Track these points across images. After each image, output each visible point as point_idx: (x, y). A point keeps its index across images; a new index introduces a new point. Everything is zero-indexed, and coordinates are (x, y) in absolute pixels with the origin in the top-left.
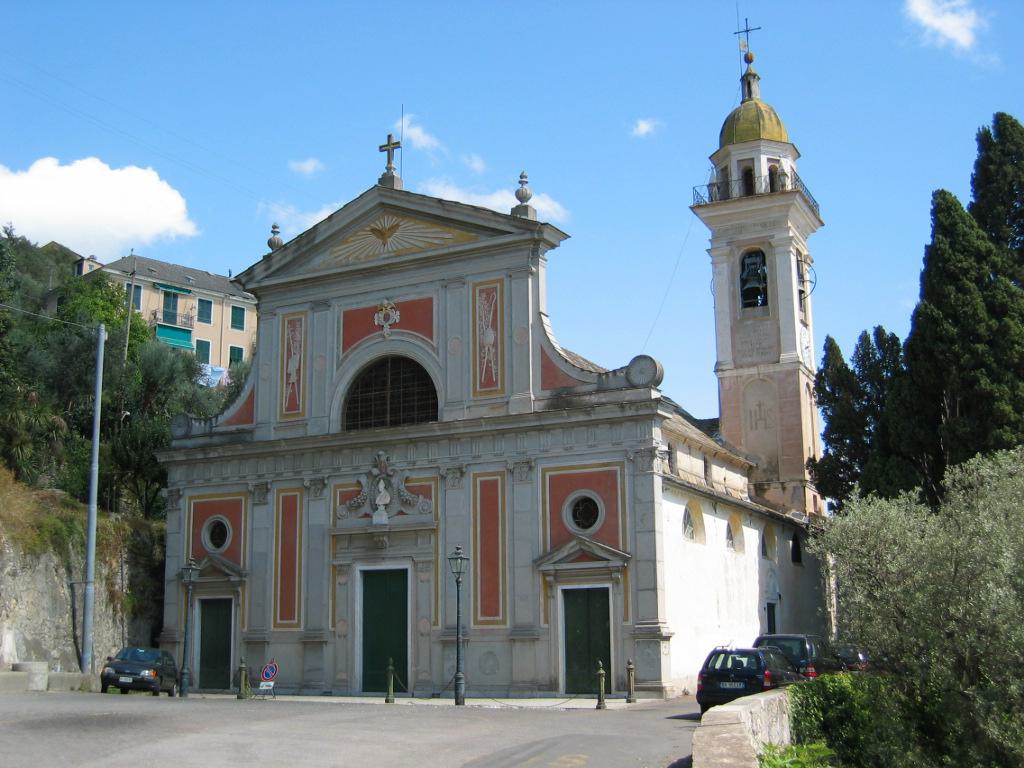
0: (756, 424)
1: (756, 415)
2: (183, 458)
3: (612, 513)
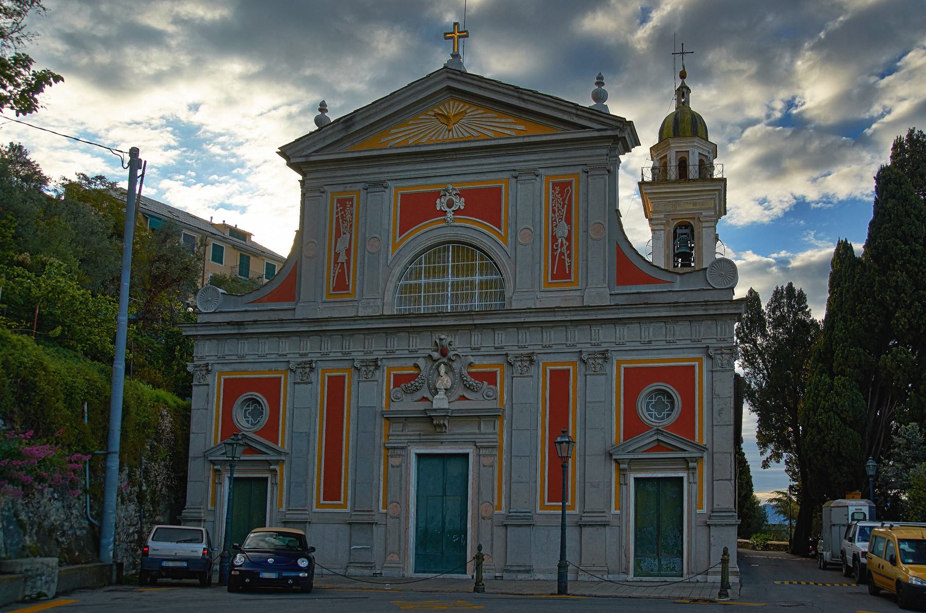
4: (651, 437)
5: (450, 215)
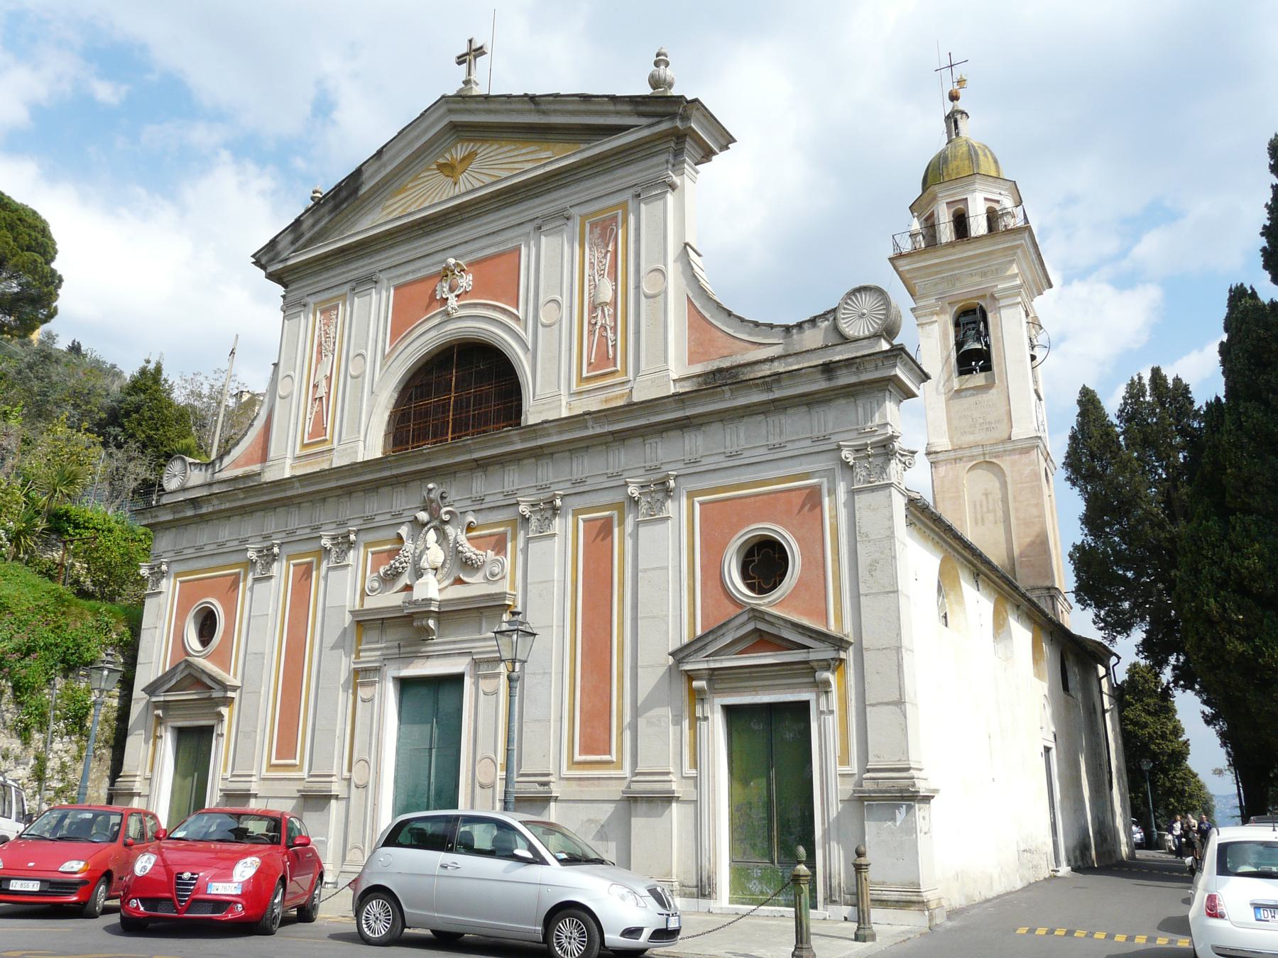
0: (982, 518)
1: (981, 506)
2: (169, 517)
3: (816, 563)
4: (743, 624)
5: (453, 302)
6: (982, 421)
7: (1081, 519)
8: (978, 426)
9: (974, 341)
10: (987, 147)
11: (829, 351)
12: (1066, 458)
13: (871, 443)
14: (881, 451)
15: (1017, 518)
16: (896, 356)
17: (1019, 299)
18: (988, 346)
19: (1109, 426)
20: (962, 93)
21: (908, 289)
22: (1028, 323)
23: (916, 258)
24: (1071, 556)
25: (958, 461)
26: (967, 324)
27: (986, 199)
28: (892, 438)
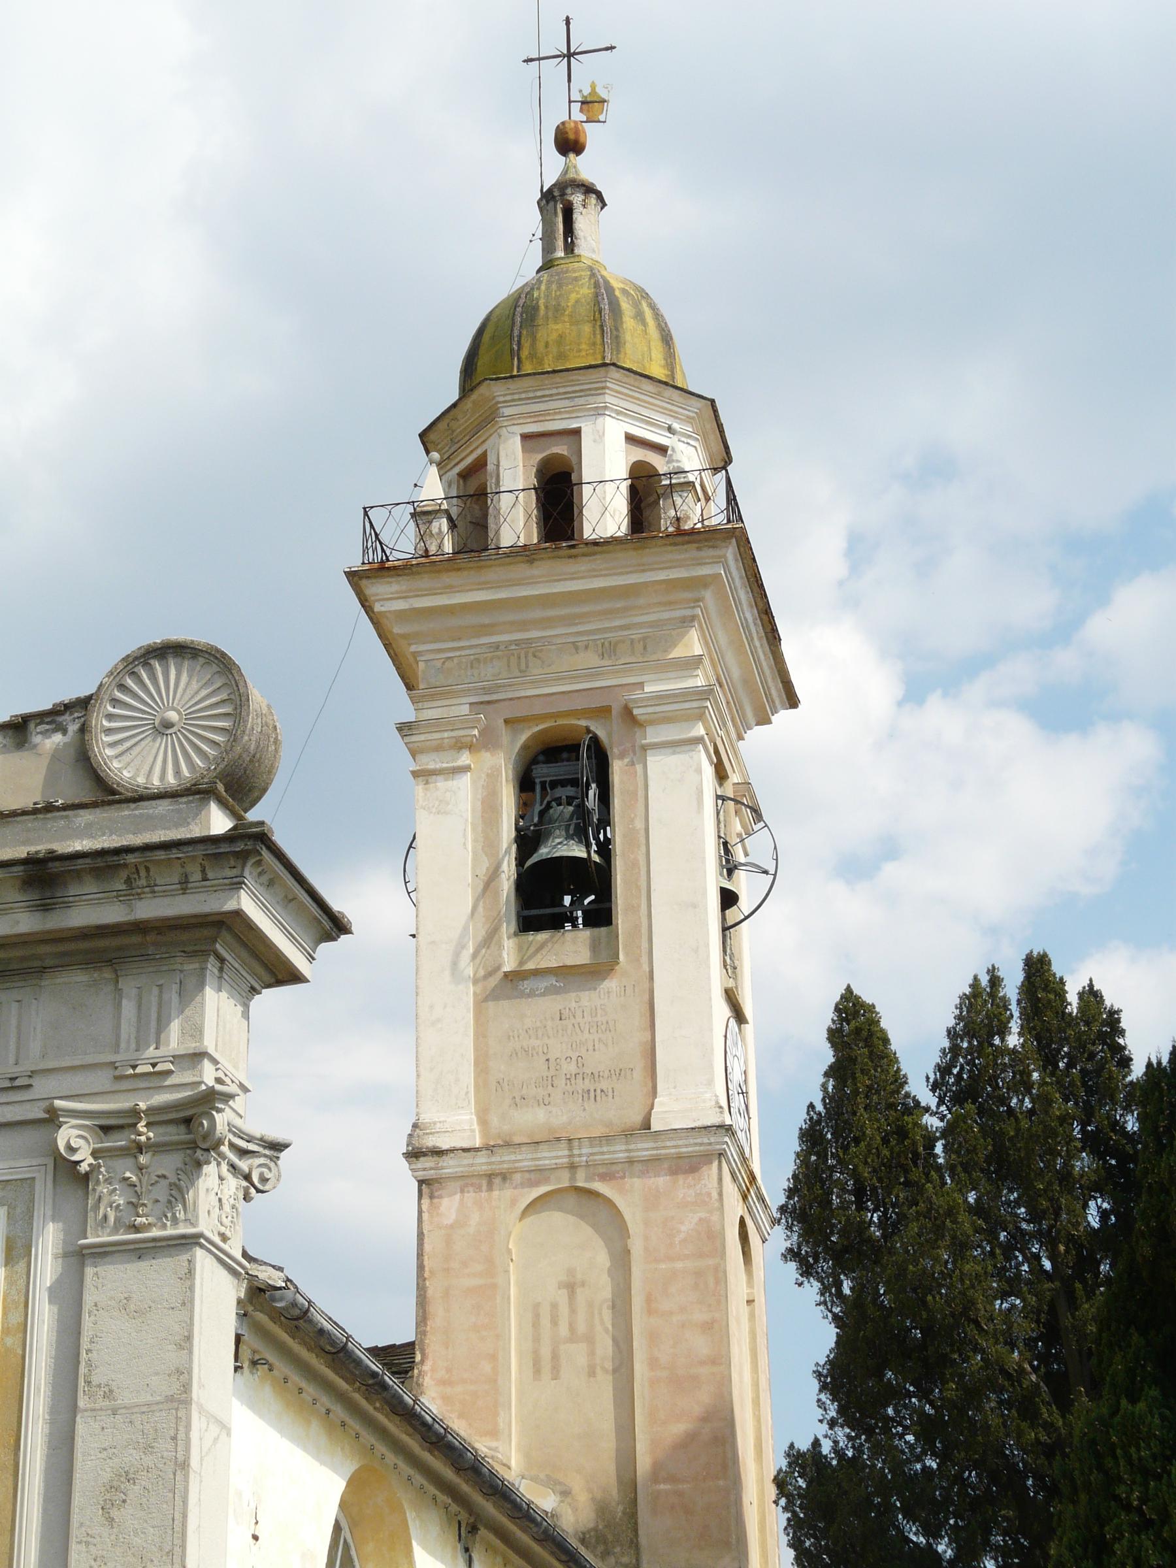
0: (555, 1357)
1: (554, 1322)
6: (572, 1068)
7: (818, 1375)
8: (561, 1082)
9: (569, 837)
10: (646, 296)
11: (57, 823)
12: (791, 1193)
13: (151, 1111)
14: (176, 1134)
15: (653, 1363)
16: (243, 856)
17: (700, 730)
18: (605, 849)
19: (908, 1111)
20: (592, 133)
21: (398, 669)
22: (723, 798)
23: (425, 582)
24: (780, 1482)
25: (497, 1181)
26: (554, 784)
27: (631, 439)
28: (211, 1099)
